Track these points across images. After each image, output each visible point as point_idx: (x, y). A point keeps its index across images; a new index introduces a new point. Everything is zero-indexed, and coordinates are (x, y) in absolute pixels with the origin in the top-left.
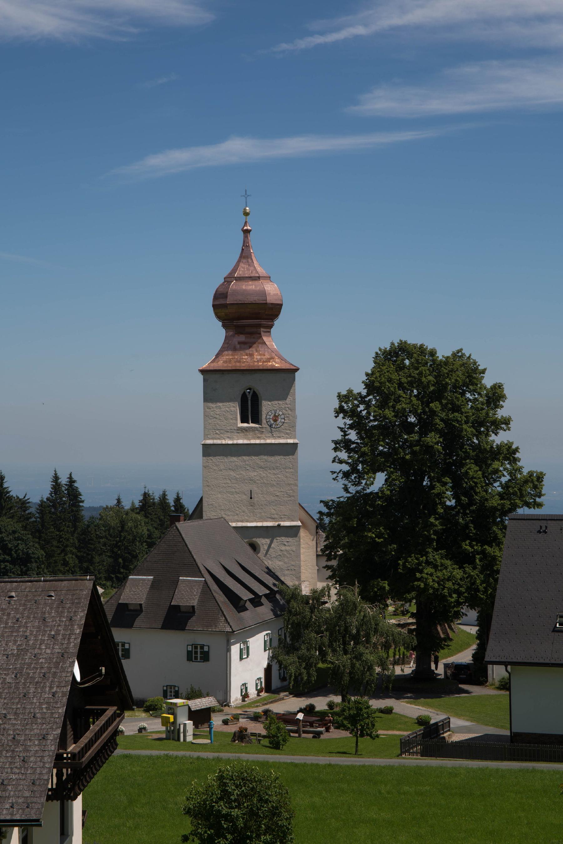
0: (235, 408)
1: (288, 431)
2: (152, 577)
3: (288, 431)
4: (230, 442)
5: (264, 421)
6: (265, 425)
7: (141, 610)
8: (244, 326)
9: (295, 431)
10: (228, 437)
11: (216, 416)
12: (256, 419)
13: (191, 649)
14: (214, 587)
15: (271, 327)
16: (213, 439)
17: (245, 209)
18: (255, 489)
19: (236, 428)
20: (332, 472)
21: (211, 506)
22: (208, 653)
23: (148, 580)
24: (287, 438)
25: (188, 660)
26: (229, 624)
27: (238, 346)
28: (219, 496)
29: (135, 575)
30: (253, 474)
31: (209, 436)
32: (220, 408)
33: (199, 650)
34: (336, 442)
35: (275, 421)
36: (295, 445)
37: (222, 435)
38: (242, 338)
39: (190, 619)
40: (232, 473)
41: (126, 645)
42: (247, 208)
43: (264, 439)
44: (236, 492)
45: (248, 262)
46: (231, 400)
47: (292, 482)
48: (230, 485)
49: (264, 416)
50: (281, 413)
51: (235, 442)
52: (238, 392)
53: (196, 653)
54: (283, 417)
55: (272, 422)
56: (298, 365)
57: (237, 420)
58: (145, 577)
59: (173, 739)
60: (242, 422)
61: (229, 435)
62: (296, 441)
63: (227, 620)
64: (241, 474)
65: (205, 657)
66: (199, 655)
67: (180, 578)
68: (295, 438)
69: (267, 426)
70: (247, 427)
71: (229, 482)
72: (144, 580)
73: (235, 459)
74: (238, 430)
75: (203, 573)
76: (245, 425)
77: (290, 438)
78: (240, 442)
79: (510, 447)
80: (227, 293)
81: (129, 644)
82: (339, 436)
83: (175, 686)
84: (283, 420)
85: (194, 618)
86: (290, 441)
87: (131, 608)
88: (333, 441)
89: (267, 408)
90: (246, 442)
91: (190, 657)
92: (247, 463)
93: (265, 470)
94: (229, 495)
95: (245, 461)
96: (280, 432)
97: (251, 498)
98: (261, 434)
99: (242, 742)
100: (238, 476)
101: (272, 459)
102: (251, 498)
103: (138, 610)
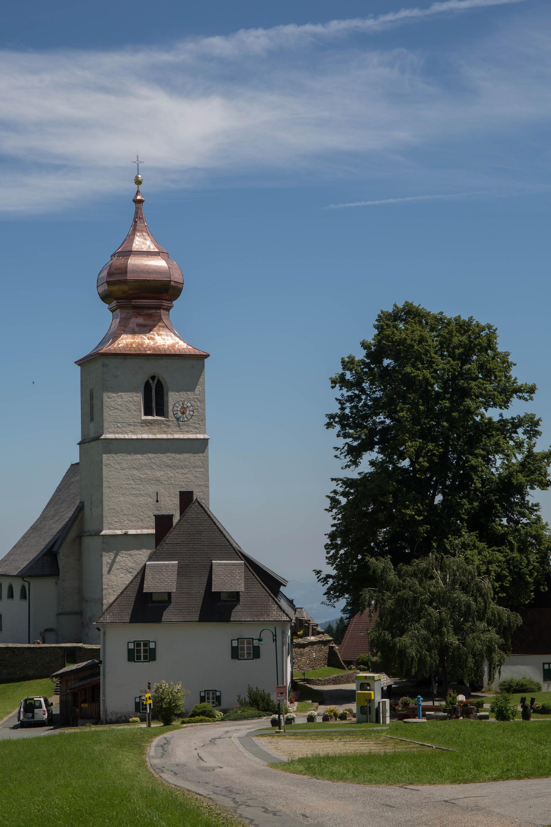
0: (138, 398)
1: (197, 426)
2: (177, 562)
3: (197, 426)
4: (134, 437)
5: (171, 413)
6: (171, 418)
7: (169, 601)
9: (205, 425)
10: (131, 432)
11: (117, 407)
12: (161, 411)
13: (236, 645)
15: (168, 309)
16: (114, 433)
17: (137, 177)
18: (161, 490)
19: (139, 421)
20: (334, 448)
21: (113, 511)
23: (173, 565)
24: (196, 433)
26: (284, 612)
27: (137, 329)
28: (122, 499)
29: (154, 561)
30: (159, 474)
31: (109, 430)
32: (122, 398)
34: (332, 417)
35: (183, 413)
36: (206, 441)
37: (124, 429)
38: (140, 320)
39: (233, 609)
40: (136, 472)
42: (140, 176)
43: (171, 434)
44: (141, 494)
45: (143, 235)
46: (133, 389)
47: (202, 483)
48: (133, 486)
49: (170, 408)
50: (189, 405)
51: (139, 437)
52: (141, 379)
54: (191, 409)
55: (180, 415)
56: (208, 352)
57: (141, 412)
58: (167, 562)
59: (371, 722)
60: (146, 414)
61: (132, 428)
62: (206, 436)
63: (281, 608)
64: (146, 474)
65: (256, 653)
67: (213, 562)
68: (204, 433)
69: (174, 419)
70: (152, 420)
71: (132, 482)
72: (168, 565)
73: (139, 456)
74: (141, 423)
76: (150, 418)
77: (200, 433)
78: (145, 436)
79: (532, 418)
80: (126, 268)
82: (335, 409)
83: (216, 691)
84: (191, 413)
85: (238, 608)
86: (201, 436)
87: (155, 598)
88: (327, 415)
89: (174, 399)
90: (151, 436)
91: (235, 654)
92: (153, 461)
93: (173, 469)
94: (132, 498)
95: (150, 459)
96: (188, 426)
97: (157, 501)
98: (168, 428)
99: (469, 718)
100: (142, 476)
101: (178, 456)
102: (157, 501)
103: (166, 600)
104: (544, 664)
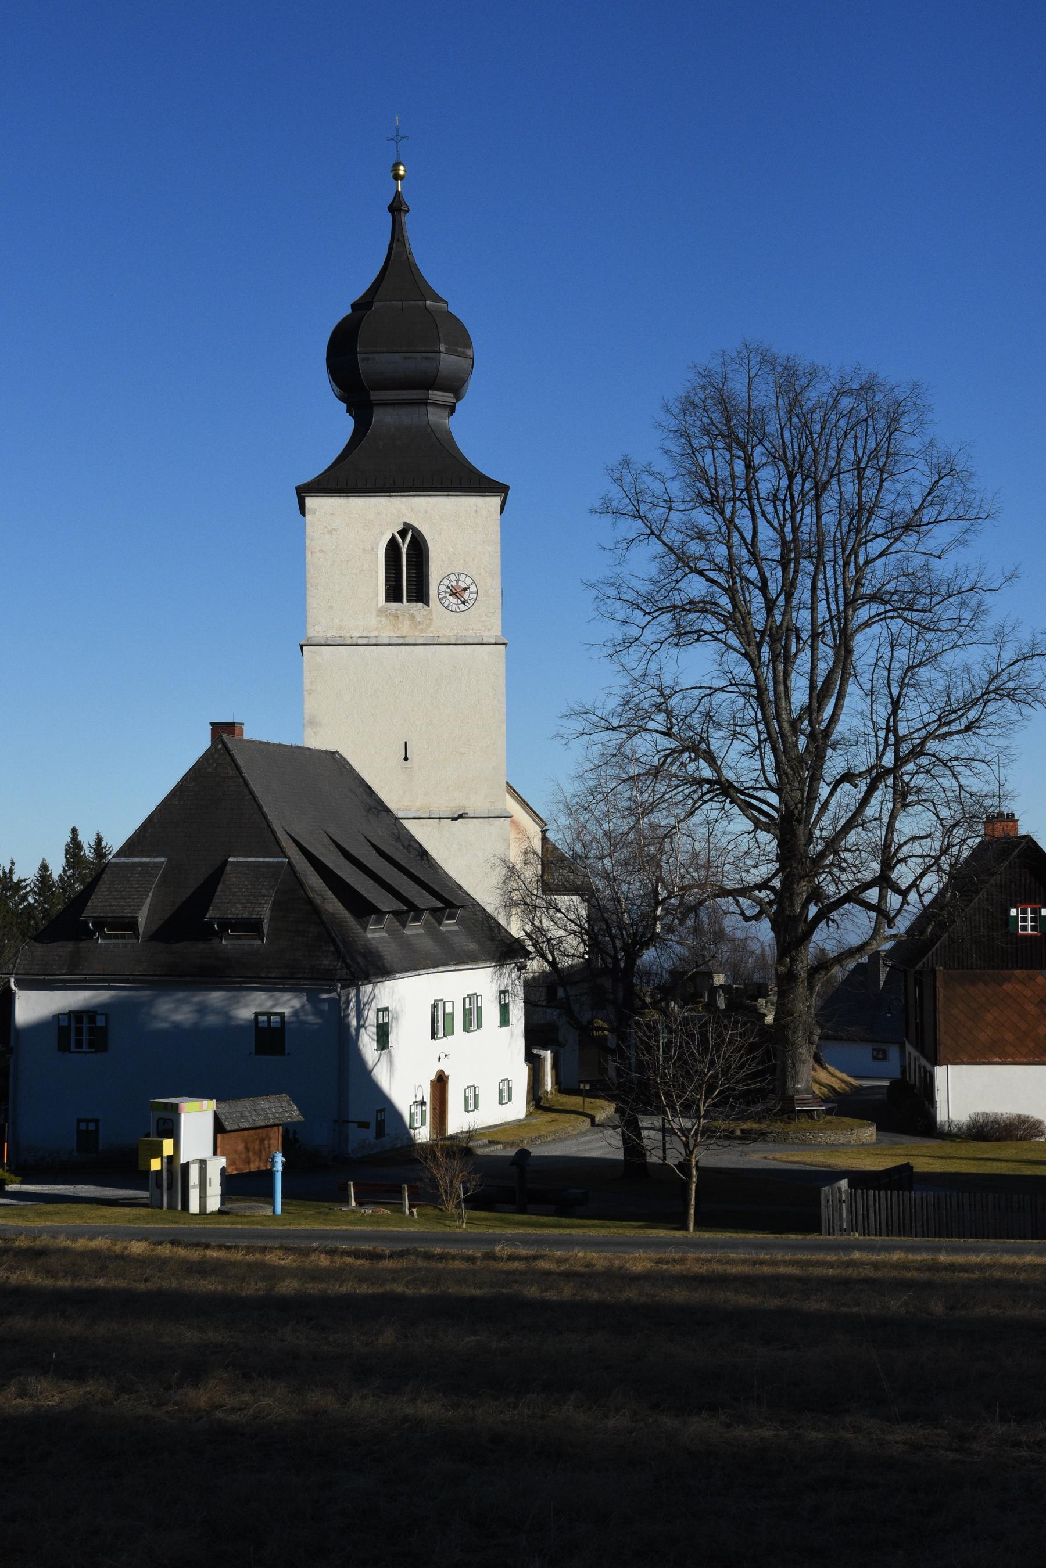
8: (800, 452)
14: (314, 880)
22: (104, 1030)
23: (157, 866)
25: (59, 1049)
33: (85, 1025)
41: (99, 1018)
53: (79, 1031)
66: (85, 1037)
67: (231, 859)
75: (284, 844)
81: (106, 1015)
104: (79, 1121)
